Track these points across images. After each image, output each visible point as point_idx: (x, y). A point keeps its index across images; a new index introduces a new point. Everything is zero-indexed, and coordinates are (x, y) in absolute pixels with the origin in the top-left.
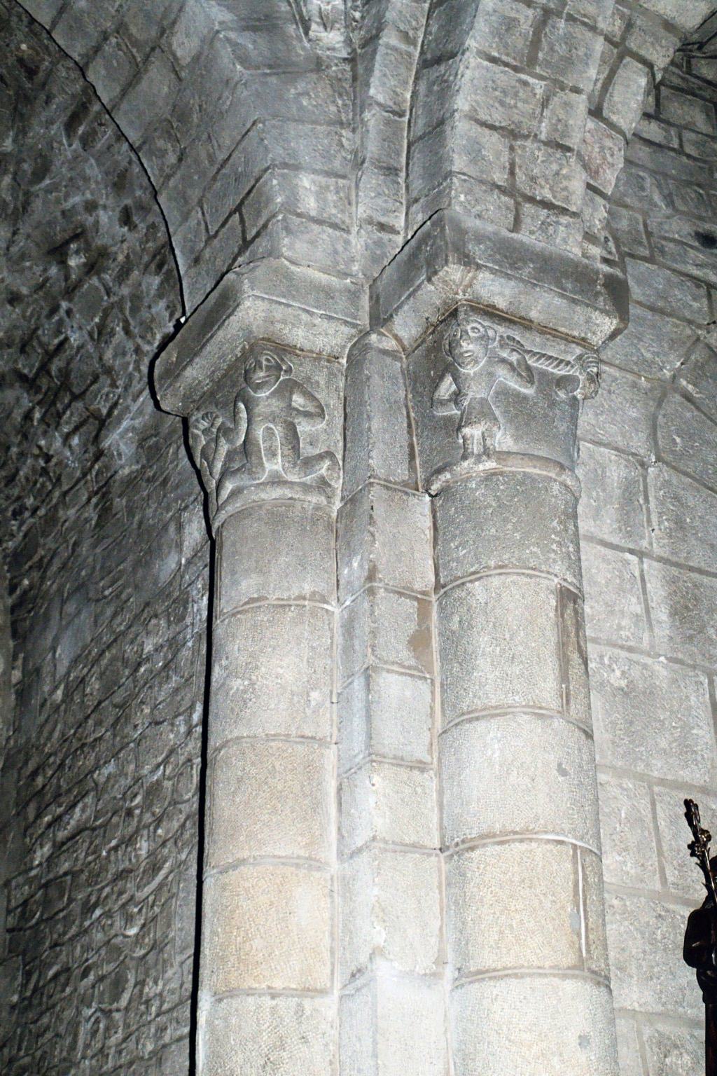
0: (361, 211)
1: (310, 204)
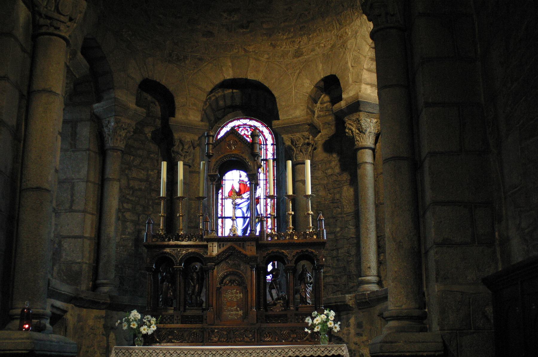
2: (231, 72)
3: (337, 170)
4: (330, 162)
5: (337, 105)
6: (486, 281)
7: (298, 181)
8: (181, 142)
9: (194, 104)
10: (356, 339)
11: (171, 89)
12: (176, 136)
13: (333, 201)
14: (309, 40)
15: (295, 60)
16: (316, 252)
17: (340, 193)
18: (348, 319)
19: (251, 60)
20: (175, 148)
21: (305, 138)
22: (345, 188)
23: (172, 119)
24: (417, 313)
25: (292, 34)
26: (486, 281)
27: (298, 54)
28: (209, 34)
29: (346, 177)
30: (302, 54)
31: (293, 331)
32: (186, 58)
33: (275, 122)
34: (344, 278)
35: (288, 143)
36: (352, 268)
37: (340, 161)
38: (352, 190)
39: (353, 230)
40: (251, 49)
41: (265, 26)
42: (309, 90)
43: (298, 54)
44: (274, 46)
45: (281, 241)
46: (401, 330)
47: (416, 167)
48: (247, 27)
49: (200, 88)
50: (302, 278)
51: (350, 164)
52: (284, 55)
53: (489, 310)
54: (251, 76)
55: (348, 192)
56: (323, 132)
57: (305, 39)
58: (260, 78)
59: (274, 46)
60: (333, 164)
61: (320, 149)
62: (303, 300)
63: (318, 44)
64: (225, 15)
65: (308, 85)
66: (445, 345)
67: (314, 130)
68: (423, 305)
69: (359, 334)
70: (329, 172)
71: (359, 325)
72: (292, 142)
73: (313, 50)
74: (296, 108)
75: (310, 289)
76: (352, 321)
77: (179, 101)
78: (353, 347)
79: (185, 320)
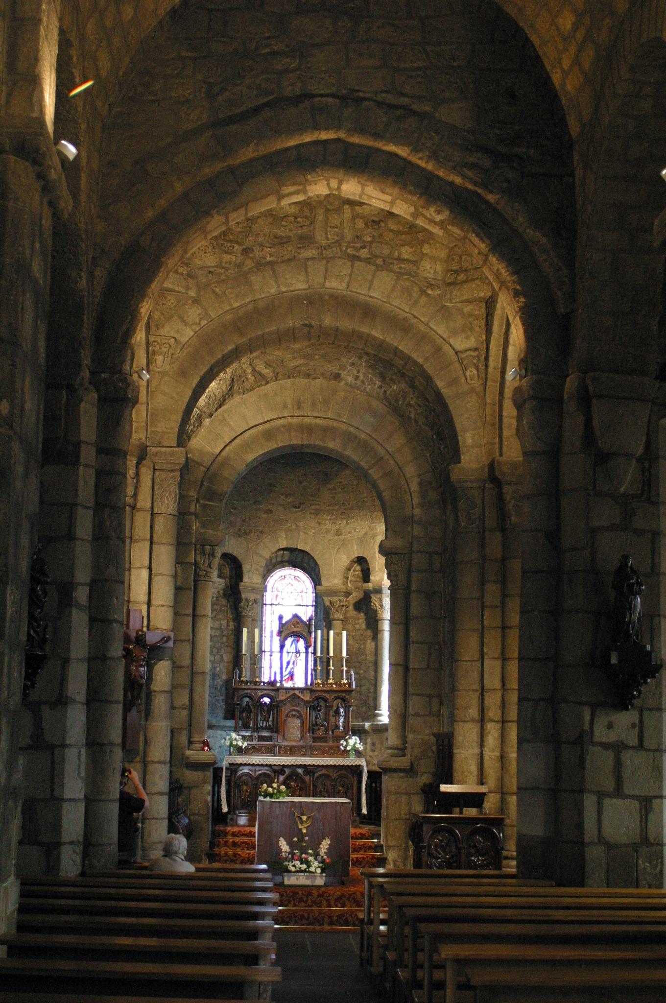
0: (485, 441)
1: (470, 441)
2: (285, 542)
3: (364, 626)
4: (358, 619)
5: (366, 584)
6: (434, 735)
7: (338, 645)
8: (247, 600)
9: (257, 570)
10: (371, 754)
11: (240, 558)
12: (243, 596)
13: (359, 649)
14: (348, 524)
15: (336, 537)
16: (347, 697)
17: (365, 644)
18: (366, 740)
19: (301, 533)
20: (242, 604)
21: (341, 601)
22: (369, 642)
23: (241, 583)
24: (400, 747)
25: (334, 517)
26: (434, 735)
27: (338, 533)
28: (269, 511)
29: (369, 633)
30: (341, 534)
31: (331, 748)
32: (251, 531)
33: (318, 587)
34: (364, 709)
35: (328, 603)
36: (371, 702)
37: (366, 619)
38: (373, 644)
39: (372, 673)
40: (301, 524)
41: (313, 507)
42: (346, 564)
43: (338, 533)
44: (320, 524)
45: (326, 688)
46: (393, 756)
47: (407, 669)
48: (299, 507)
49: (261, 556)
50: (337, 713)
51: (373, 623)
52: (328, 531)
53: (434, 748)
54: (300, 547)
55: (370, 645)
56: (354, 594)
57: (344, 521)
58: (307, 549)
59: (320, 524)
60: (361, 621)
61: (351, 608)
62: (337, 727)
63: (355, 529)
64: (282, 497)
65: (344, 560)
66: (412, 764)
67: (348, 594)
68: (405, 742)
69: (373, 751)
70: (358, 626)
71: (373, 744)
72: (331, 602)
73: (350, 532)
74: (335, 577)
75: (342, 720)
76: (369, 740)
77: (246, 568)
78: (368, 758)
79: (261, 738)
